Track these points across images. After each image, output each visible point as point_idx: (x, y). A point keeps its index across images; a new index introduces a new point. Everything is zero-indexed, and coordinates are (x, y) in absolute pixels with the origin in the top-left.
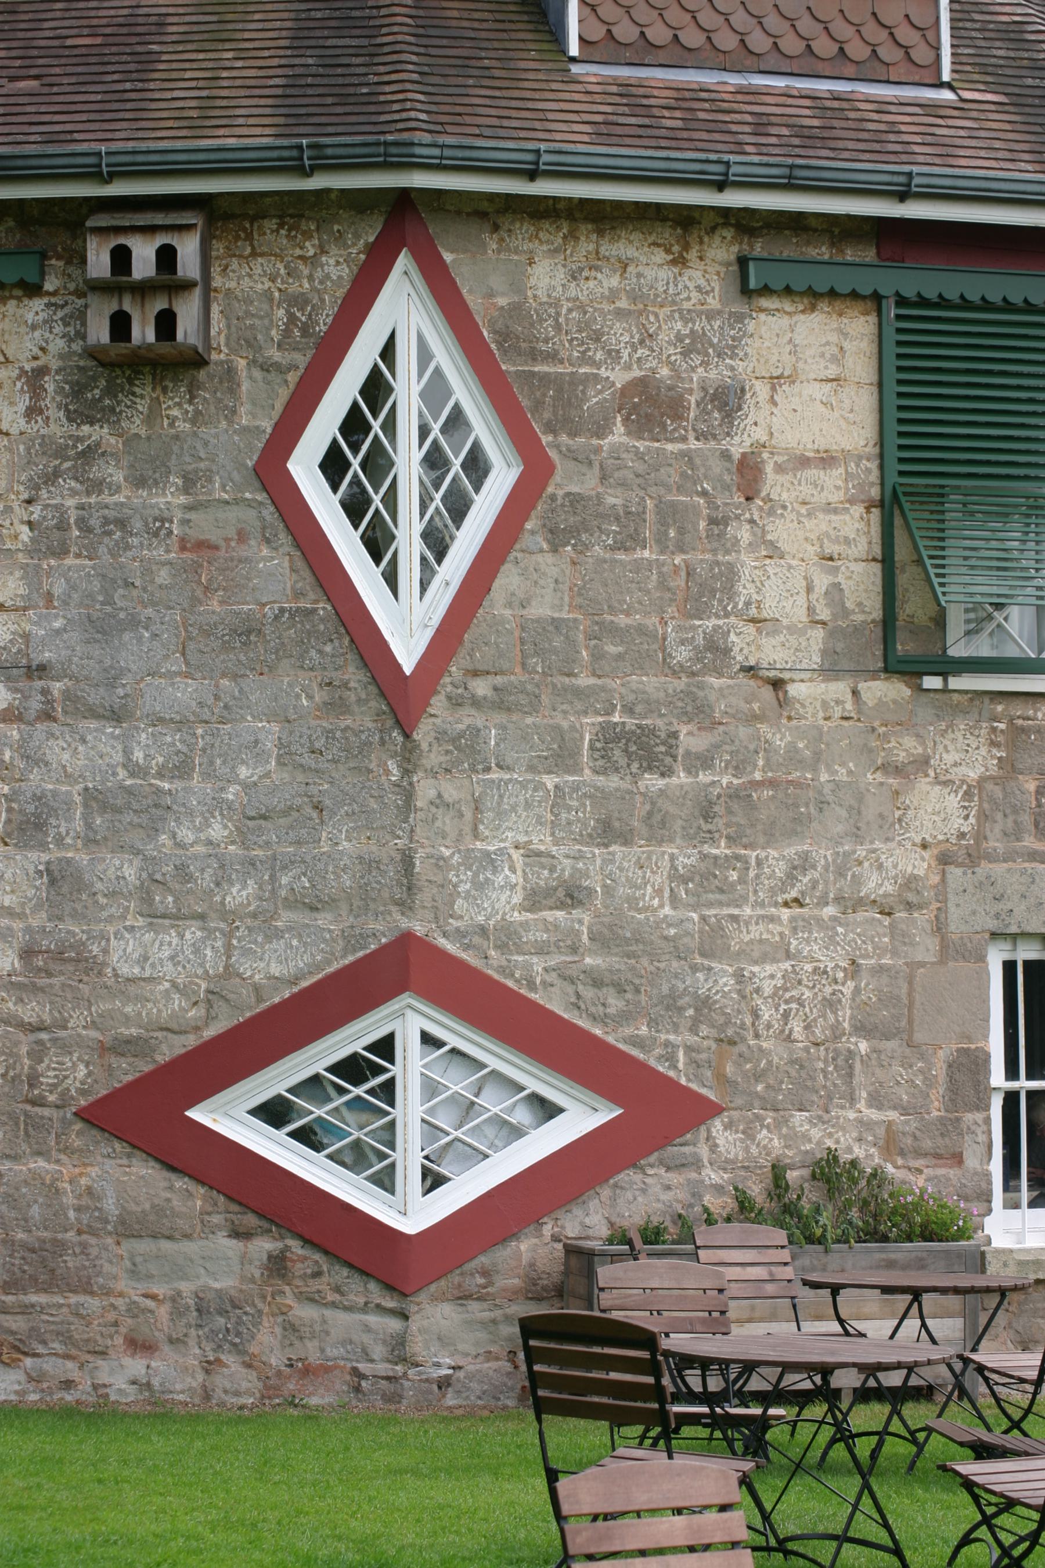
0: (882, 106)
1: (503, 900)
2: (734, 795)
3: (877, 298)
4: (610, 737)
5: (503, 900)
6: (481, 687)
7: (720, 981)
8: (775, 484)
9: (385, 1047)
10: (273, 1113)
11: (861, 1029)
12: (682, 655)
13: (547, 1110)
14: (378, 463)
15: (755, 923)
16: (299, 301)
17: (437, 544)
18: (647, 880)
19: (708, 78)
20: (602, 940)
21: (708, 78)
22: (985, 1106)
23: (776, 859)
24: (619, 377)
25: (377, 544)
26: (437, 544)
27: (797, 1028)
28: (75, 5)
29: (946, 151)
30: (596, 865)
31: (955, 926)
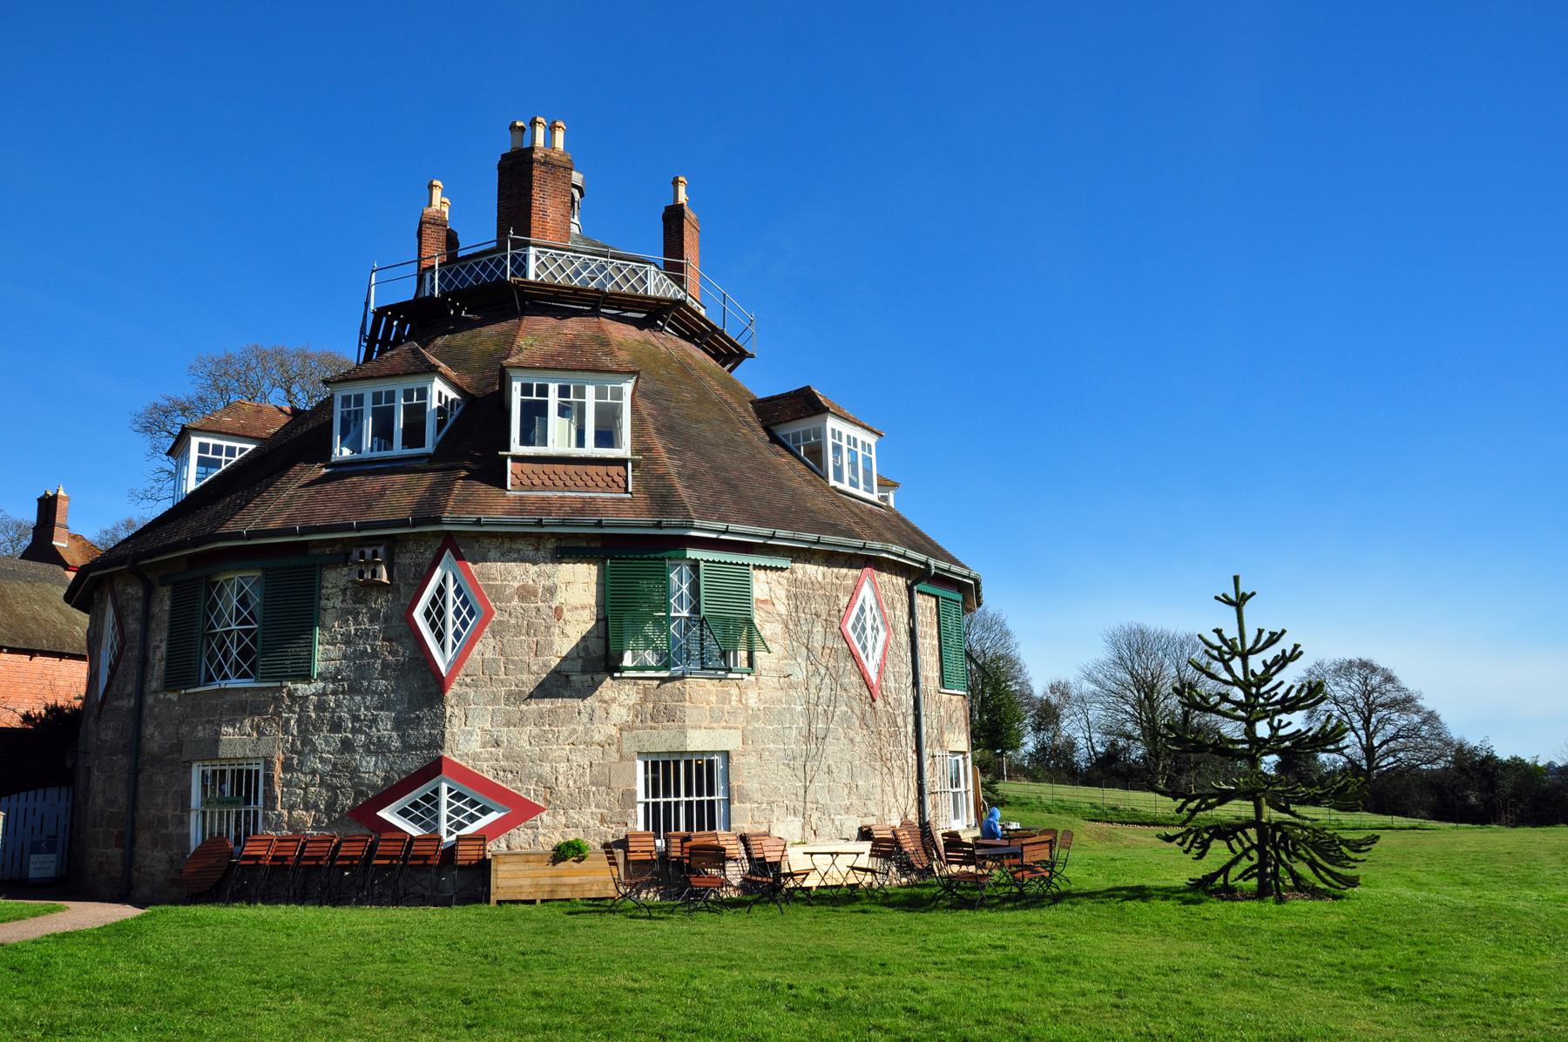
0: (605, 500)
1: (475, 746)
2: (551, 711)
3: (937, 597)
4: (509, 694)
5: (475, 746)
6: (468, 680)
7: (546, 769)
8: (567, 615)
9: (437, 791)
10: (404, 813)
11: (592, 783)
12: (535, 668)
13: (485, 811)
14: (441, 613)
15: (559, 751)
16: (418, 565)
18: (522, 739)
19: (550, 494)
20: (506, 758)
21: (550, 494)
22: (634, 807)
23: (565, 730)
24: (516, 584)
25: (440, 636)
27: (571, 783)
28: (732, 527)
29: (619, 512)
30: (504, 733)
31: (625, 750)
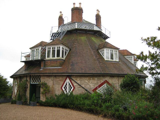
17: (66, 84)
25: (69, 84)
26: (66, 84)
